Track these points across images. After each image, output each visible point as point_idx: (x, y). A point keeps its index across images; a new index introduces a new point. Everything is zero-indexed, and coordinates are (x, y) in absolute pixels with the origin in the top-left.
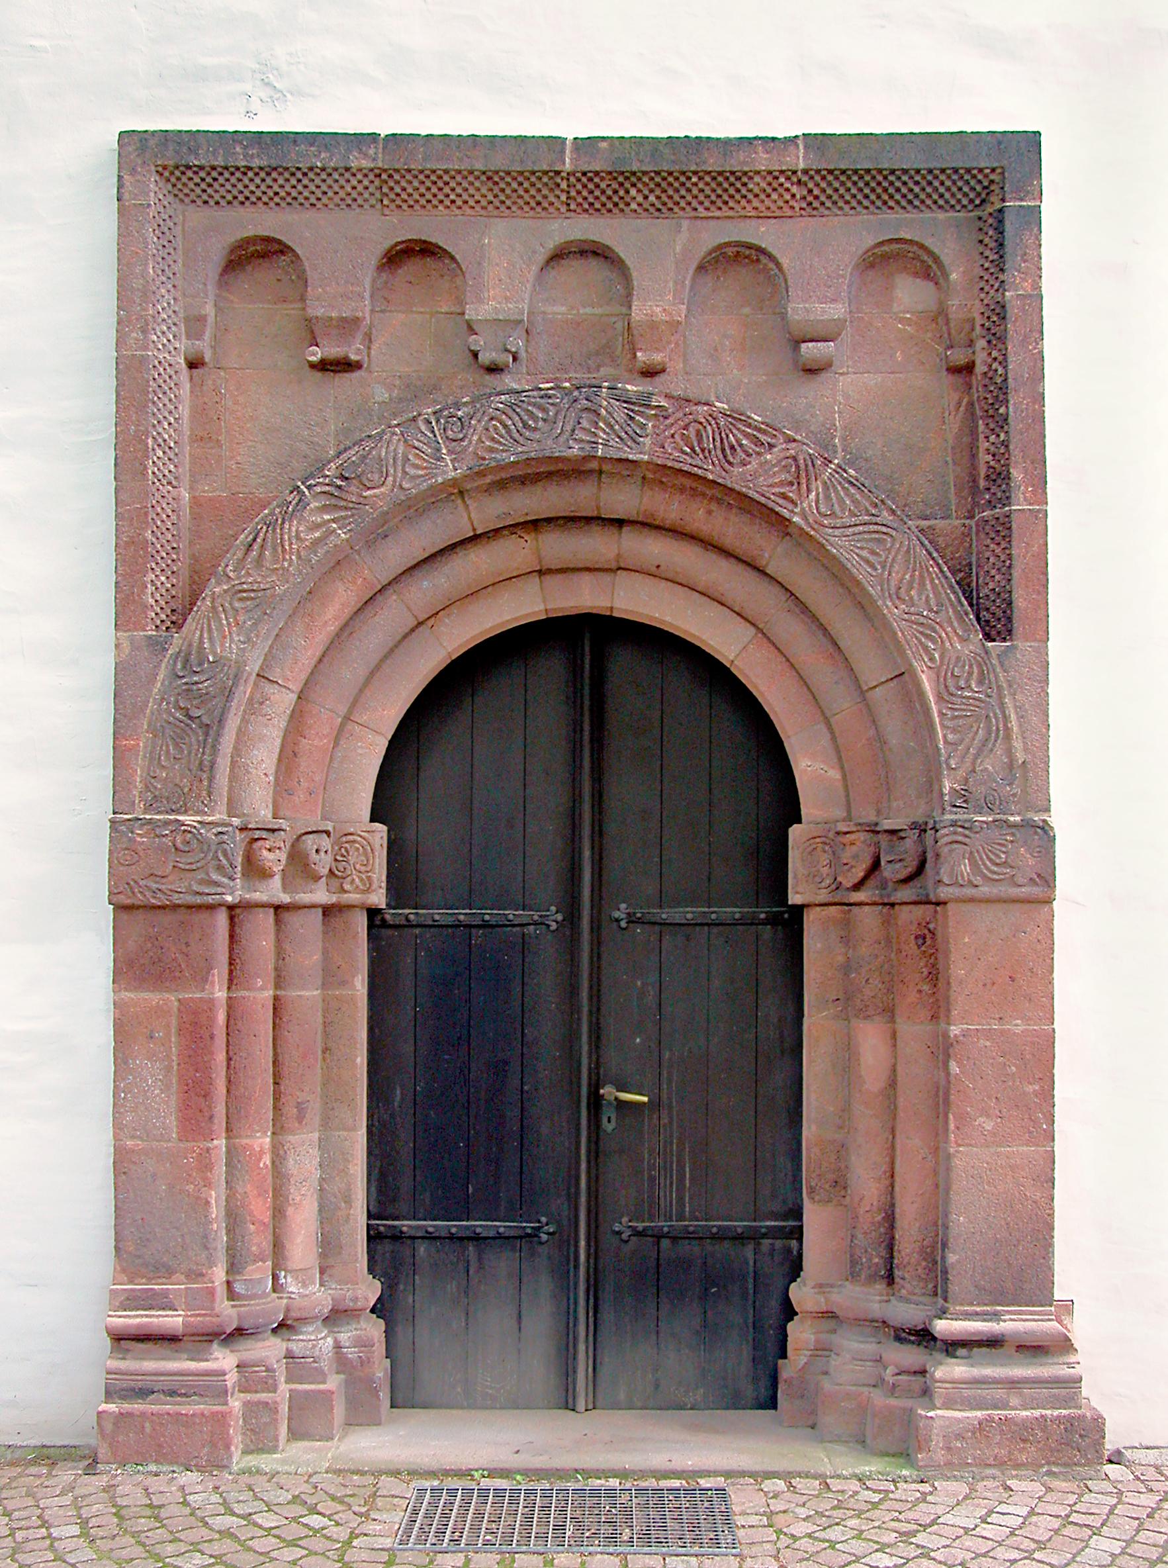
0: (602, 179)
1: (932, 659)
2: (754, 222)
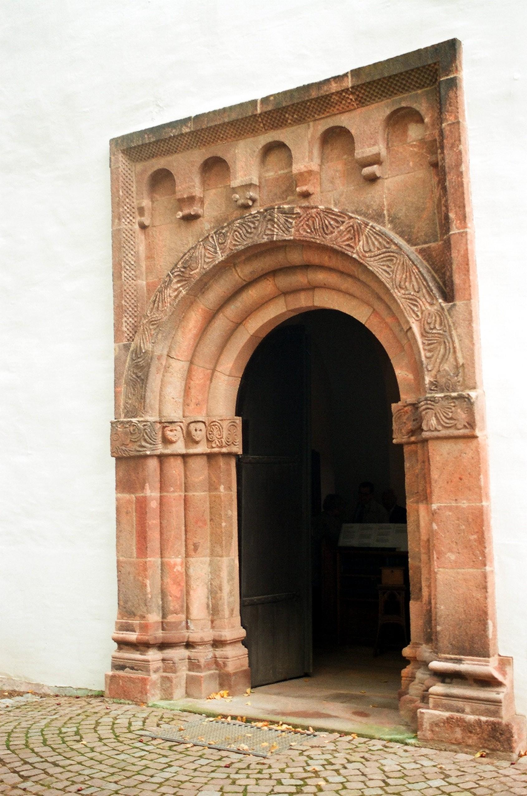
0: (273, 113)
1: (417, 316)
2: (339, 116)
